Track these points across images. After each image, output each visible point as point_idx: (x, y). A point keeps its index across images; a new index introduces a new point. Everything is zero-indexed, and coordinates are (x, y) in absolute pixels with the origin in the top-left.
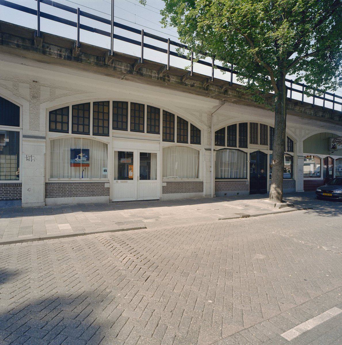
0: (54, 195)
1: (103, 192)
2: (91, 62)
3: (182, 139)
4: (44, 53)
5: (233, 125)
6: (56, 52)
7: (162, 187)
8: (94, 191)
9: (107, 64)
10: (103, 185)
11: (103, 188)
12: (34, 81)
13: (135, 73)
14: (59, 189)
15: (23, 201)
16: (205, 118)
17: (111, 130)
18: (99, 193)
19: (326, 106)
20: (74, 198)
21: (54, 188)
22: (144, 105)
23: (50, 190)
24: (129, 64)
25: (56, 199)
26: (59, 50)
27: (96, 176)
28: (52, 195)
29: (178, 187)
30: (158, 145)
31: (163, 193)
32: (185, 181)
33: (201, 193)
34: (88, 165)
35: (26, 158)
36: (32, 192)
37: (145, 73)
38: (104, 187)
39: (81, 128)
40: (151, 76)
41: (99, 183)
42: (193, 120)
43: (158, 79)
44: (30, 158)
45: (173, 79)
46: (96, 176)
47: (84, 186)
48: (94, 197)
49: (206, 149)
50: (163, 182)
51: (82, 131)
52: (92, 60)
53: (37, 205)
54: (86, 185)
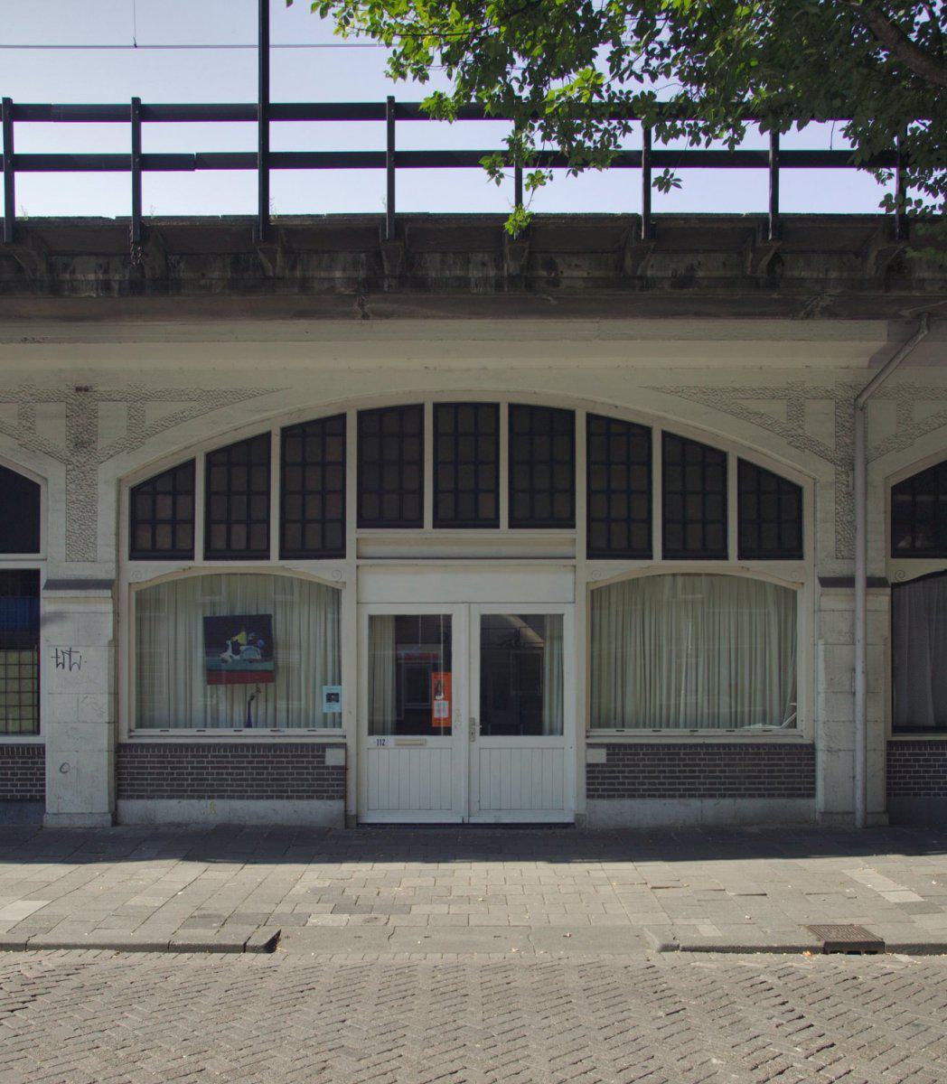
0: (146, 791)
1: (318, 785)
2: (214, 282)
3: (694, 537)
4: (55, 289)
5: (248, 443)
6: (92, 277)
7: (583, 770)
8: (285, 780)
9: (271, 274)
10: (318, 756)
11: (319, 768)
12: (78, 389)
13: (389, 286)
14: (160, 768)
15: (51, 806)
16: (821, 423)
17: (352, 532)
18: (303, 785)
19: (277, 208)
20: (209, 801)
21: (144, 762)
22: (570, 415)
23: (131, 768)
24: (363, 255)
25: (150, 804)
26: (101, 266)
27: (702, 722)
28: (140, 791)
29: (670, 771)
30: (568, 578)
31: (588, 797)
32: (708, 741)
33: (801, 803)
34: (269, 677)
35: (55, 659)
36: (76, 777)
37: (434, 275)
38: (323, 762)
39: (237, 535)
40: (464, 283)
41: (187, 749)
42: (747, 443)
43: (499, 286)
44: (67, 656)
45: (575, 272)
46: (702, 722)
47: (247, 756)
48: (285, 803)
49: (826, 582)
50: (590, 746)
51: (243, 545)
52: (216, 274)
53: (88, 822)
54: (253, 757)
